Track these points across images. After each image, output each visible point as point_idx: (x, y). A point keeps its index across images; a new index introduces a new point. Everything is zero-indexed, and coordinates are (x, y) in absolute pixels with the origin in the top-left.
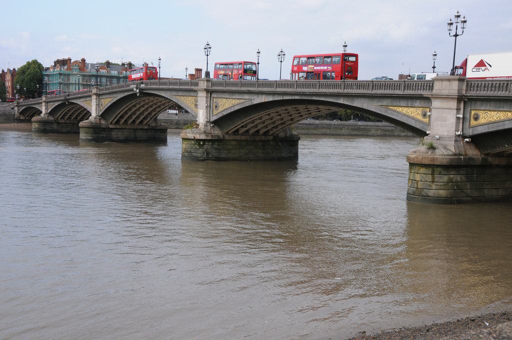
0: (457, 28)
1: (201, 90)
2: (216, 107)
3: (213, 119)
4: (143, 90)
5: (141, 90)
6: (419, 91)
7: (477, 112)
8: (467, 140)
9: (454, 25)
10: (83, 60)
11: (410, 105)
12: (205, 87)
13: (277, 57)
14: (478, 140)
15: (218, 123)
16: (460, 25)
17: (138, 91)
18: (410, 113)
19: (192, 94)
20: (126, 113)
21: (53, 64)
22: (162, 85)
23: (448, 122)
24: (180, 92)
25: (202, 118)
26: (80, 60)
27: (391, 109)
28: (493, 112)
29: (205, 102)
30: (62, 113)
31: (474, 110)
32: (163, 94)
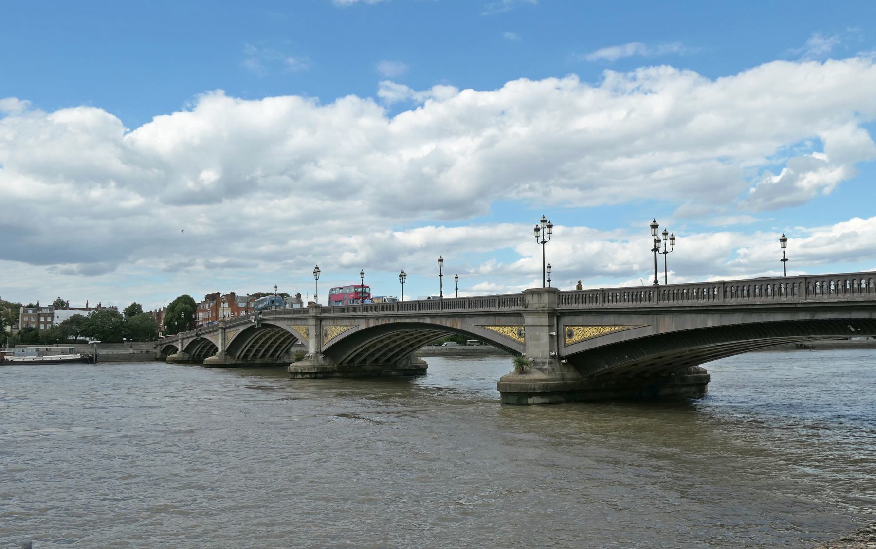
0: (665, 245)
1: (310, 317)
2: (326, 335)
3: (324, 349)
4: (262, 320)
5: (259, 321)
6: (519, 306)
7: (570, 328)
8: (564, 361)
9: (542, 230)
10: (233, 294)
11: (335, 324)
12: (314, 315)
13: (399, 278)
14: (577, 361)
15: (328, 353)
16: (668, 242)
17: (256, 322)
18: (507, 332)
19: (304, 322)
20: (252, 347)
21: (204, 300)
22: (337, 312)
23: (541, 341)
24: (297, 321)
25: (312, 349)
26: (229, 293)
27: (488, 329)
28: (586, 328)
29: (314, 331)
30: (199, 347)
31: (567, 326)
32: (278, 324)
